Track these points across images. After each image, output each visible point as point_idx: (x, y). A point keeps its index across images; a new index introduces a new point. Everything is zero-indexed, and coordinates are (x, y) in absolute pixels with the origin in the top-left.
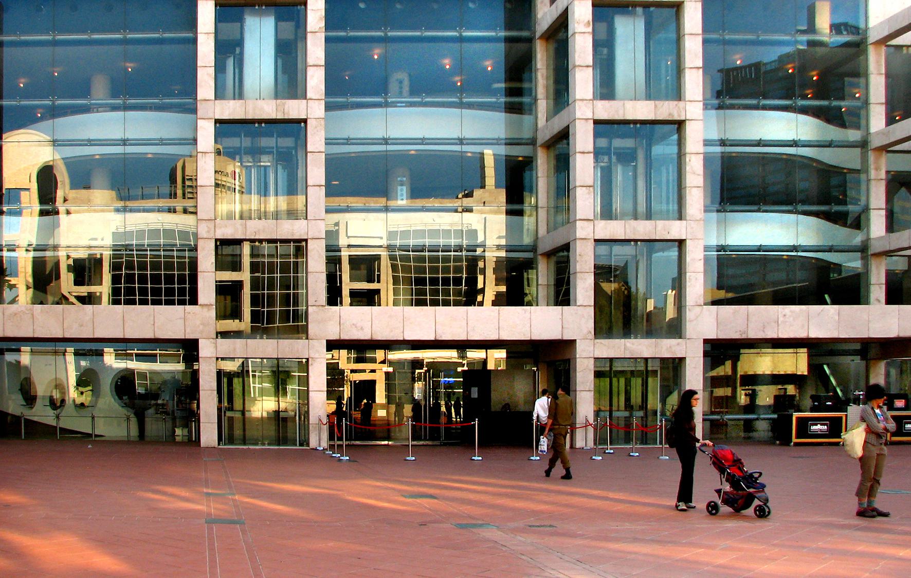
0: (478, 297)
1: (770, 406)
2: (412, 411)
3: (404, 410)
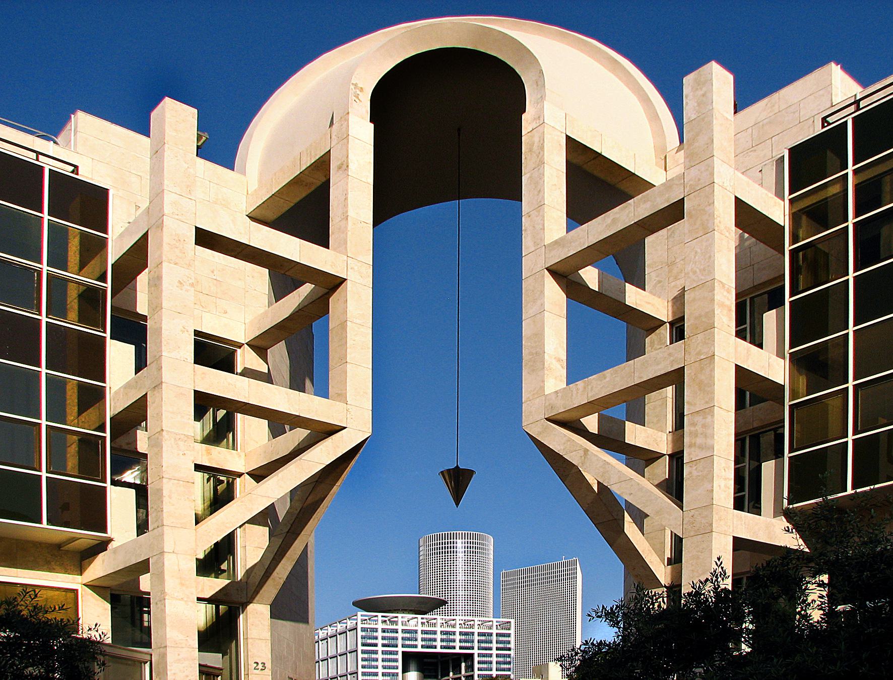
2: (372, 120)
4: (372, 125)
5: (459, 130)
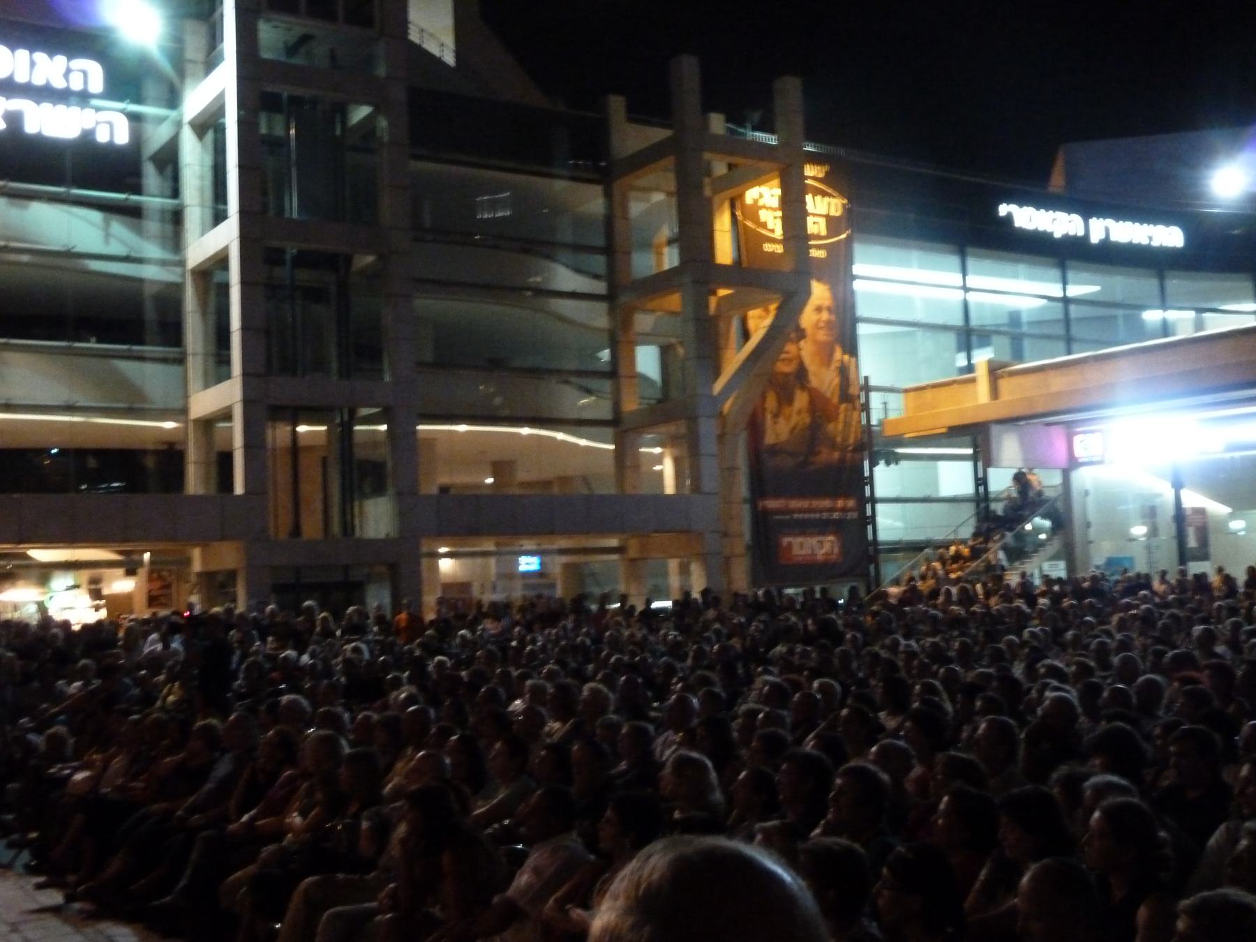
2: (1173, 487)
3: (758, 187)
5: (1031, 220)
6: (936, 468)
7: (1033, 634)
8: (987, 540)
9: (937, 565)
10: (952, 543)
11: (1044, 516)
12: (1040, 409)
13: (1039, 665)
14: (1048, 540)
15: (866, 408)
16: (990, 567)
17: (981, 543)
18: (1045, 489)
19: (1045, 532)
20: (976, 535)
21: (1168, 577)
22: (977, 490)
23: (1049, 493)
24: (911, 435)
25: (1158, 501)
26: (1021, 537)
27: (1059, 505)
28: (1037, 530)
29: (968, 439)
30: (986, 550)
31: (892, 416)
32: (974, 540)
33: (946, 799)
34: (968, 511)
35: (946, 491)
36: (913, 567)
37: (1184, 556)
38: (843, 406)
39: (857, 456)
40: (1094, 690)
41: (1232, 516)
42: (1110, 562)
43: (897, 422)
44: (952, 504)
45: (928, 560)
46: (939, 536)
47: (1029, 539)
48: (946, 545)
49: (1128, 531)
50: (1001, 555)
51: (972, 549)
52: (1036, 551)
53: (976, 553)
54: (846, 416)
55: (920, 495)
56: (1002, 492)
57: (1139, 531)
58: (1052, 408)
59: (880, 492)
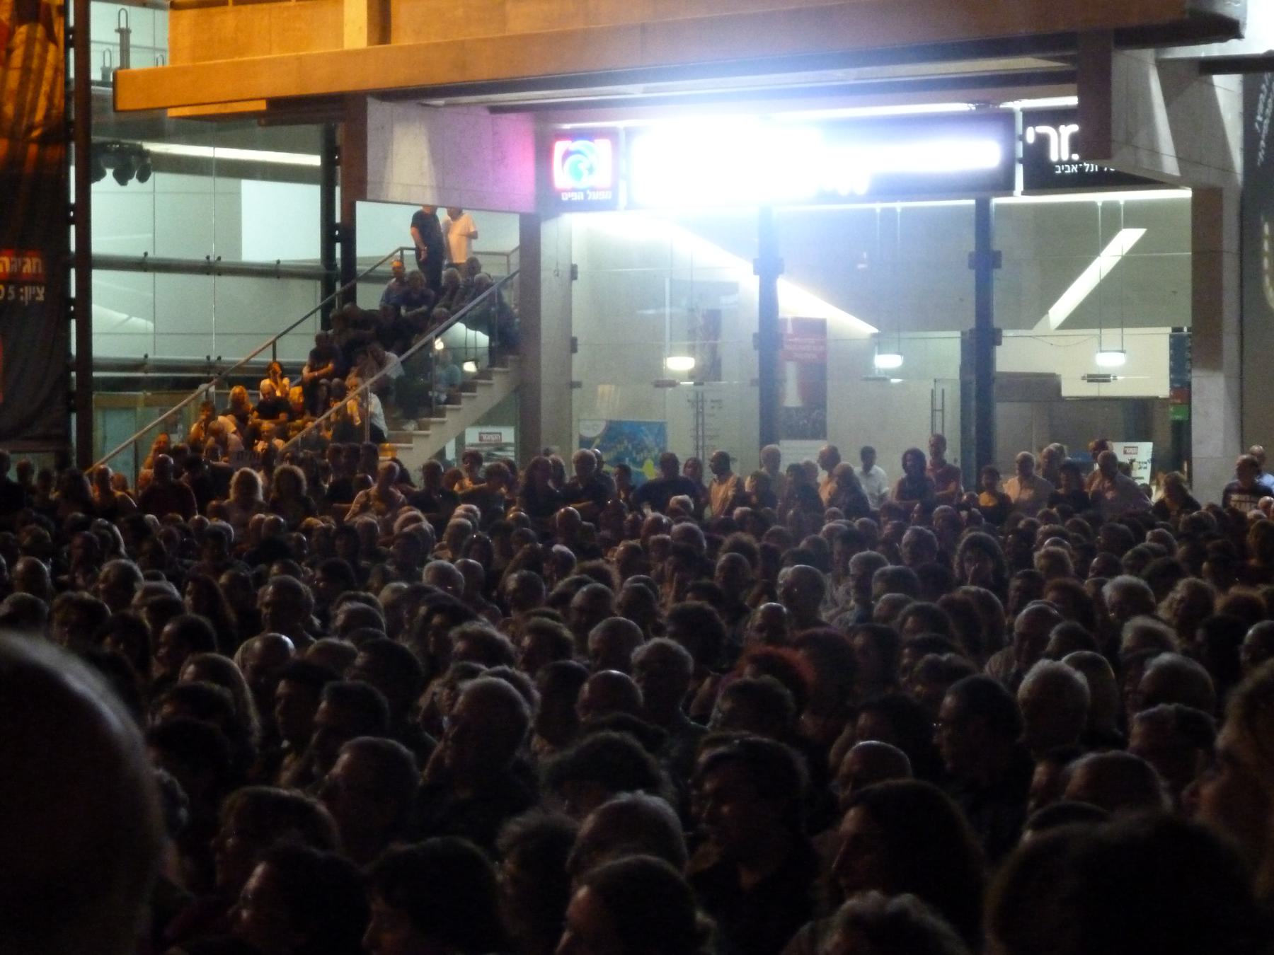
0: (1183, 515)
1: (171, 18)
2: (755, 273)
4: (757, 278)
6: (238, 194)
7: (443, 576)
8: (342, 373)
9: (227, 422)
10: (267, 371)
11: (473, 324)
12: (482, 71)
13: (453, 633)
14: (482, 374)
15: (80, 38)
16: (345, 428)
17: (330, 376)
18: (481, 260)
19: (476, 361)
20: (318, 357)
21: (736, 469)
22: (86, 428)
23: (491, 270)
24: (187, 111)
25: (726, 302)
26: (422, 364)
27: (510, 297)
28: (459, 353)
29: (314, 132)
30: (341, 393)
31: (139, 62)
32: (312, 369)
33: (259, 870)
34: (308, 296)
35: (254, 251)
36: (169, 426)
37: (769, 433)
38: (22, 31)
39: (53, 153)
40: (566, 681)
41: (879, 343)
42: (614, 432)
43: (152, 76)
44: (274, 280)
45: (210, 410)
46: (234, 354)
47: (439, 371)
48: (249, 377)
49: (660, 359)
50: (375, 404)
51: (310, 389)
52: (452, 400)
53: (316, 398)
54: (28, 57)
55: (198, 256)
56: (384, 261)
57: (680, 364)
58: (505, 73)
59: (100, 245)
